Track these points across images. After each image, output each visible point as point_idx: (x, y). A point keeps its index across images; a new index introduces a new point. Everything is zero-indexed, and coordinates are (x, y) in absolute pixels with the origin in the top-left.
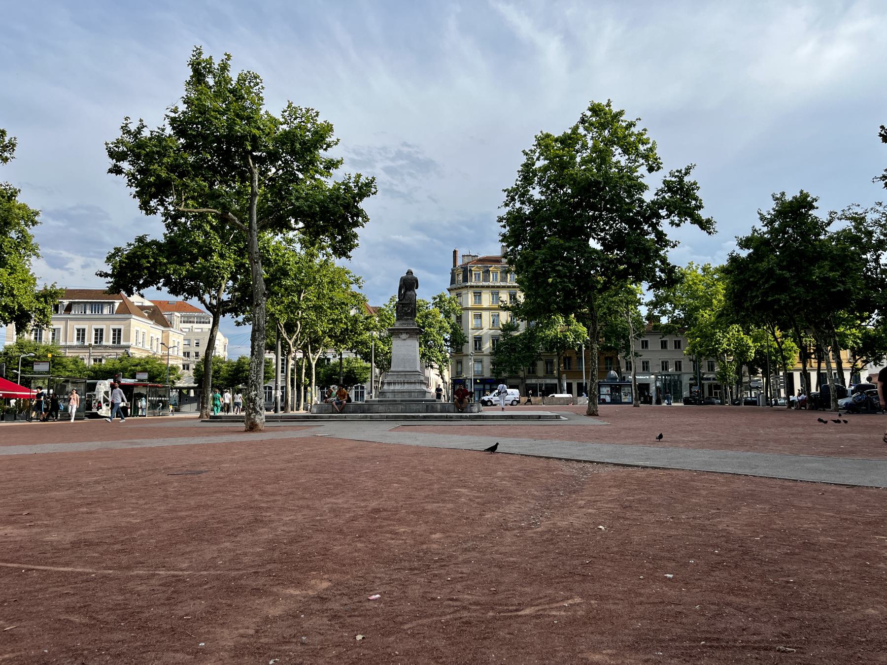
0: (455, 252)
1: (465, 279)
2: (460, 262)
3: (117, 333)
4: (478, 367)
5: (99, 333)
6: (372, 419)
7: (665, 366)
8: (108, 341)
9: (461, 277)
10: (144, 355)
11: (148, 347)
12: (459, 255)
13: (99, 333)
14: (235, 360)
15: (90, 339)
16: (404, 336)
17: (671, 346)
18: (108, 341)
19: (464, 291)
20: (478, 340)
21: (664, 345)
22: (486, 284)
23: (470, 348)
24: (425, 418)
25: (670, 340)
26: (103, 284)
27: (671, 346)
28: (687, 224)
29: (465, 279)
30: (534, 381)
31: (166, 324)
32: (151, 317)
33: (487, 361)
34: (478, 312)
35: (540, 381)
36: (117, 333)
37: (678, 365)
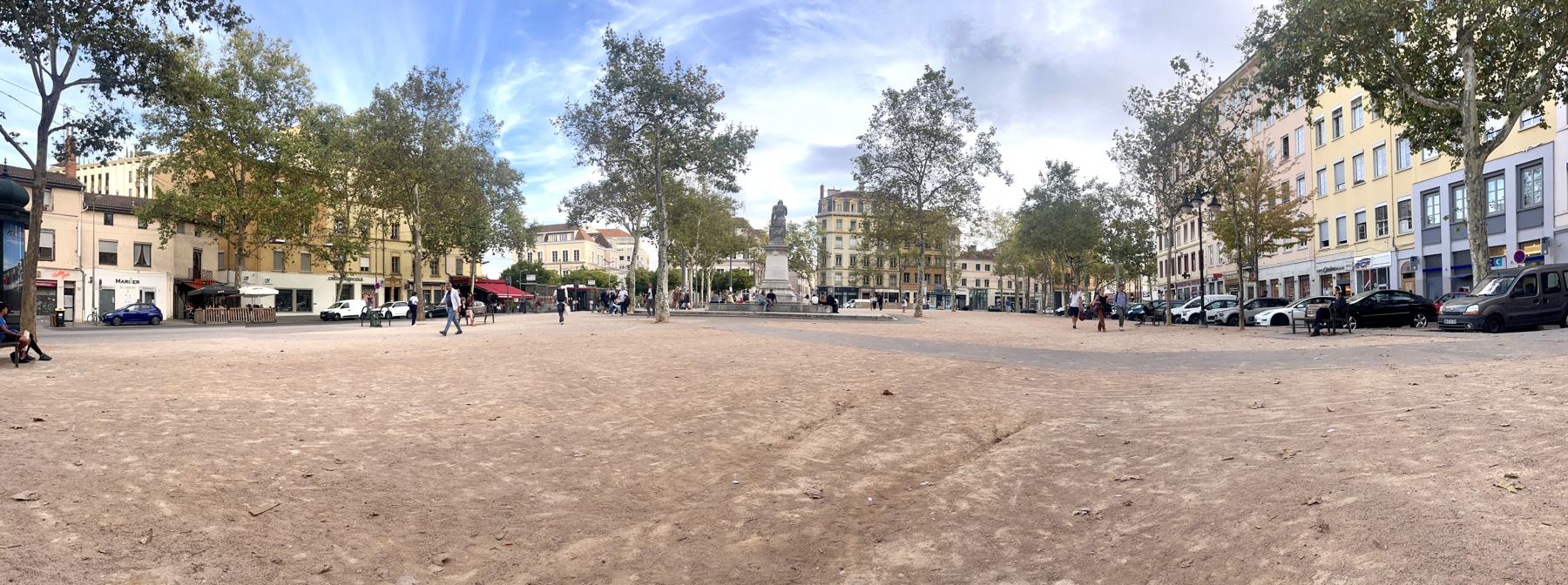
0: (822, 187)
1: (830, 209)
2: (826, 195)
3: (577, 253)
4: (838, 278)
5: (565, 253)
6: (748, 316)
7: (978, 282)
8: (571, 257)
9: (826, 207)
10: (593, 268)
11: (596, 262)
12: (826, 189)
13: (565, 253)
14: (502, 152)
15: (560, 256)
16: (775, 252)
17: (982, 268)
18: (571, 257)
19: (828, 219)
20: (839, 258)
21: (978, 267)
22: (846, 213)
23: (832, 262)
24: (789, 316)
25: (983, 264)
26: (563, 219)
27: (982, 268)
28: (993, 175)
29: (830, 209)
30: (881, 291)
31: (607, 245)
32: (597, 241)
33: (846, 274)
34: (839, 235)
35: (885, 291)
36: (577, 253)
37: (987, 282)
